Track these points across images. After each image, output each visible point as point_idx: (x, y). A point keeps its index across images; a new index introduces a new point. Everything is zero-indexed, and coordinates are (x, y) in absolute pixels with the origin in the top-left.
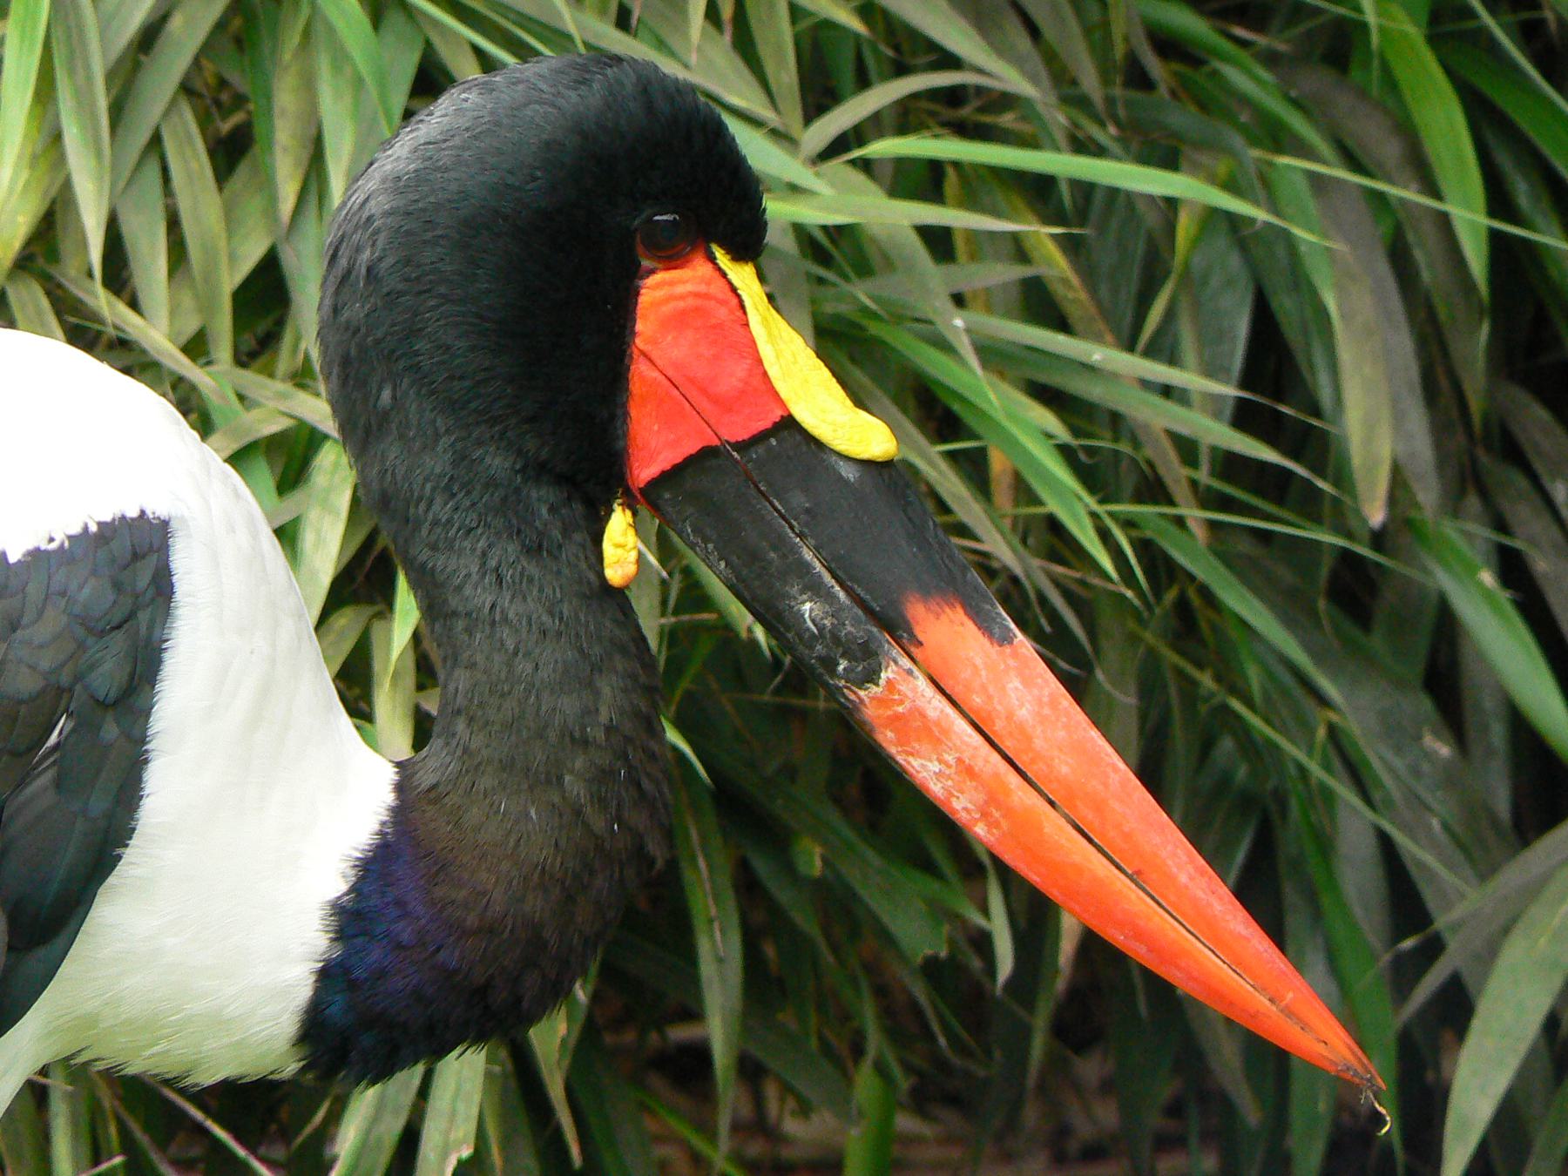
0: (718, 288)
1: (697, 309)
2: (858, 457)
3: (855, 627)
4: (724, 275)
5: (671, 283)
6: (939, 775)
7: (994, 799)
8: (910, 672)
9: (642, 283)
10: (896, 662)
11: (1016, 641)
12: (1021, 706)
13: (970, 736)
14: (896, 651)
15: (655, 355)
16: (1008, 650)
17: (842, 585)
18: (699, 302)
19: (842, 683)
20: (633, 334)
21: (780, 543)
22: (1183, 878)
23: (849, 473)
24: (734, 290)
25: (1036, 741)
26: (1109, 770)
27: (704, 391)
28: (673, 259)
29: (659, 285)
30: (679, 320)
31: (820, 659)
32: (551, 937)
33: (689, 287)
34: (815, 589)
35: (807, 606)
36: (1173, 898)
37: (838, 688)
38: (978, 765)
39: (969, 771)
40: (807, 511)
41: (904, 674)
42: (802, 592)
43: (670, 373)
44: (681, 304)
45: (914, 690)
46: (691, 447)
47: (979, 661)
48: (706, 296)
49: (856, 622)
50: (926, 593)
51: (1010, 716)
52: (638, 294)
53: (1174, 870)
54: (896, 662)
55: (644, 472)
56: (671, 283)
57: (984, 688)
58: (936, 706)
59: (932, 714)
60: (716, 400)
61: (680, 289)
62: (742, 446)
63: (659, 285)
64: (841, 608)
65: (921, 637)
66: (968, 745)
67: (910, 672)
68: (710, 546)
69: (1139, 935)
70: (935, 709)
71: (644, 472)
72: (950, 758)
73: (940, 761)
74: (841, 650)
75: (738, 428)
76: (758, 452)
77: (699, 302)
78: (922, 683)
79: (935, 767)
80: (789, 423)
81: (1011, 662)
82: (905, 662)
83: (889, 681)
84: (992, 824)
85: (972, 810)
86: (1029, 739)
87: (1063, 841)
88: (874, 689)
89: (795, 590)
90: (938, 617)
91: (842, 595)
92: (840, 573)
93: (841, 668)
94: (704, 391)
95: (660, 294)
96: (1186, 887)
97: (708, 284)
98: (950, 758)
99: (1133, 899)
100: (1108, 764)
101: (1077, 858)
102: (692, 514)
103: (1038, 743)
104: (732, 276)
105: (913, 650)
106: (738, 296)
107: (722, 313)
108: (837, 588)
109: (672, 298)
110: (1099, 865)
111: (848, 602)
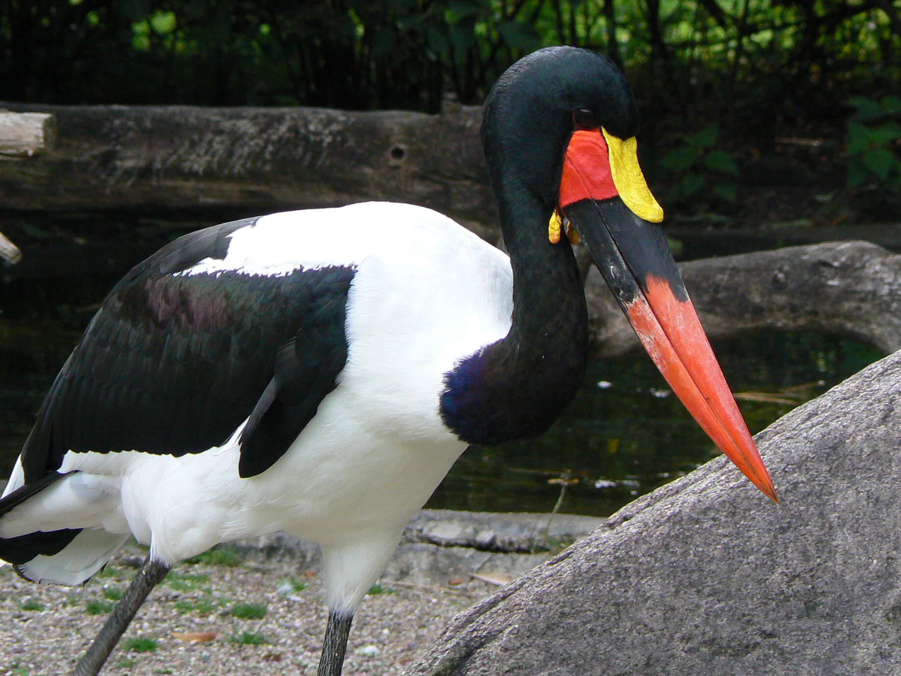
0: (601, 143)
1: (591, 147)
2: (643, 218)
3: (628, 279)
4: (604, 139)
5: (584, 135)
6: (649, 342)
7: (664, 356)
8: (643, 301)
9: (573, 132)
10: (639, 297)
11: (687, 302)
12: (680, 325)
13: (660, 331)
14: (640, 292)
15: (573, 160)
16: (682, 304)
17: (626, 264)
18: (593, 145)
19: (621, 299)
20: (566, 150)
21: (605, 240)
22: (723, 405)
23: (638, 223)
24: (607, 145)
25: (682, 340)
26: (707, 359)
27: (588, 178)
28: (589, 127)
29: (578, 135)
30: (585, 150)
31: (615, 288)
32: (293, 344)
33: (590, 139)
34: (616, 262)
35: (612, 267)
36: (718, 411)
37: (621, 301)
38: (661, 343)
39: (658, 344)
40: (618, 232)
41: (642, 302)
42: (611, 261)
43: (578, 168)
44: (586, 144)
45: (644, 308)
46: (581, 197)
47: (668, 304)
48: (596, 144)
49: (628, 278)
50: (655, 275)
51: (675, 328)
52: (571, 136)
53: (721, 401)
54: (639, 297)
55: (565, 202)
56: (584, 135)
57: (668, 315)
58: (650, 316)
59: (648, 319)
60: (592, 182)
61: (587, 139)
62: (600, 202)
63: (578, 135)
64: (624, 271)
65: (649, 290)
66: (659, 334)
67: (643, 301)
68: (584, 236)
69: (706, 422)
70: (650, 317)
71: (565, 202)
72: (652, 338)
73: (650, 338)
74: (621, 287)
75: (598, 195)
76: (604, 206)
77: (593, 145)
78: (647, 306)
79: (648, 339)
80: (617, 199)
81: (682, 308)
82: (643, 298)
83: (636, 303)
84: (663, 366)
85: (182, 273)
86: (680, 338)
87: (685, 379)
88: (631, 305)
89: (609, 260)
90: (657, 284)
91: (624, 266)
92: (626, 259)
93: (621, 293)
94: (588, 178)
95: (579, 138)
96: (724, 408)
97: (598, 140)
98: (652, 338)
99: (704, 407)
100: (707, 356)
101: (688, 386)
102: (174, 44)
103: (683, 341)
104: (607, 139)
105: (647, 295)
106: (608, 148)
107: (600, 151)
108: (623, 263)
109: (582, 141)
110: (695, 391)
111: (626, 269)
